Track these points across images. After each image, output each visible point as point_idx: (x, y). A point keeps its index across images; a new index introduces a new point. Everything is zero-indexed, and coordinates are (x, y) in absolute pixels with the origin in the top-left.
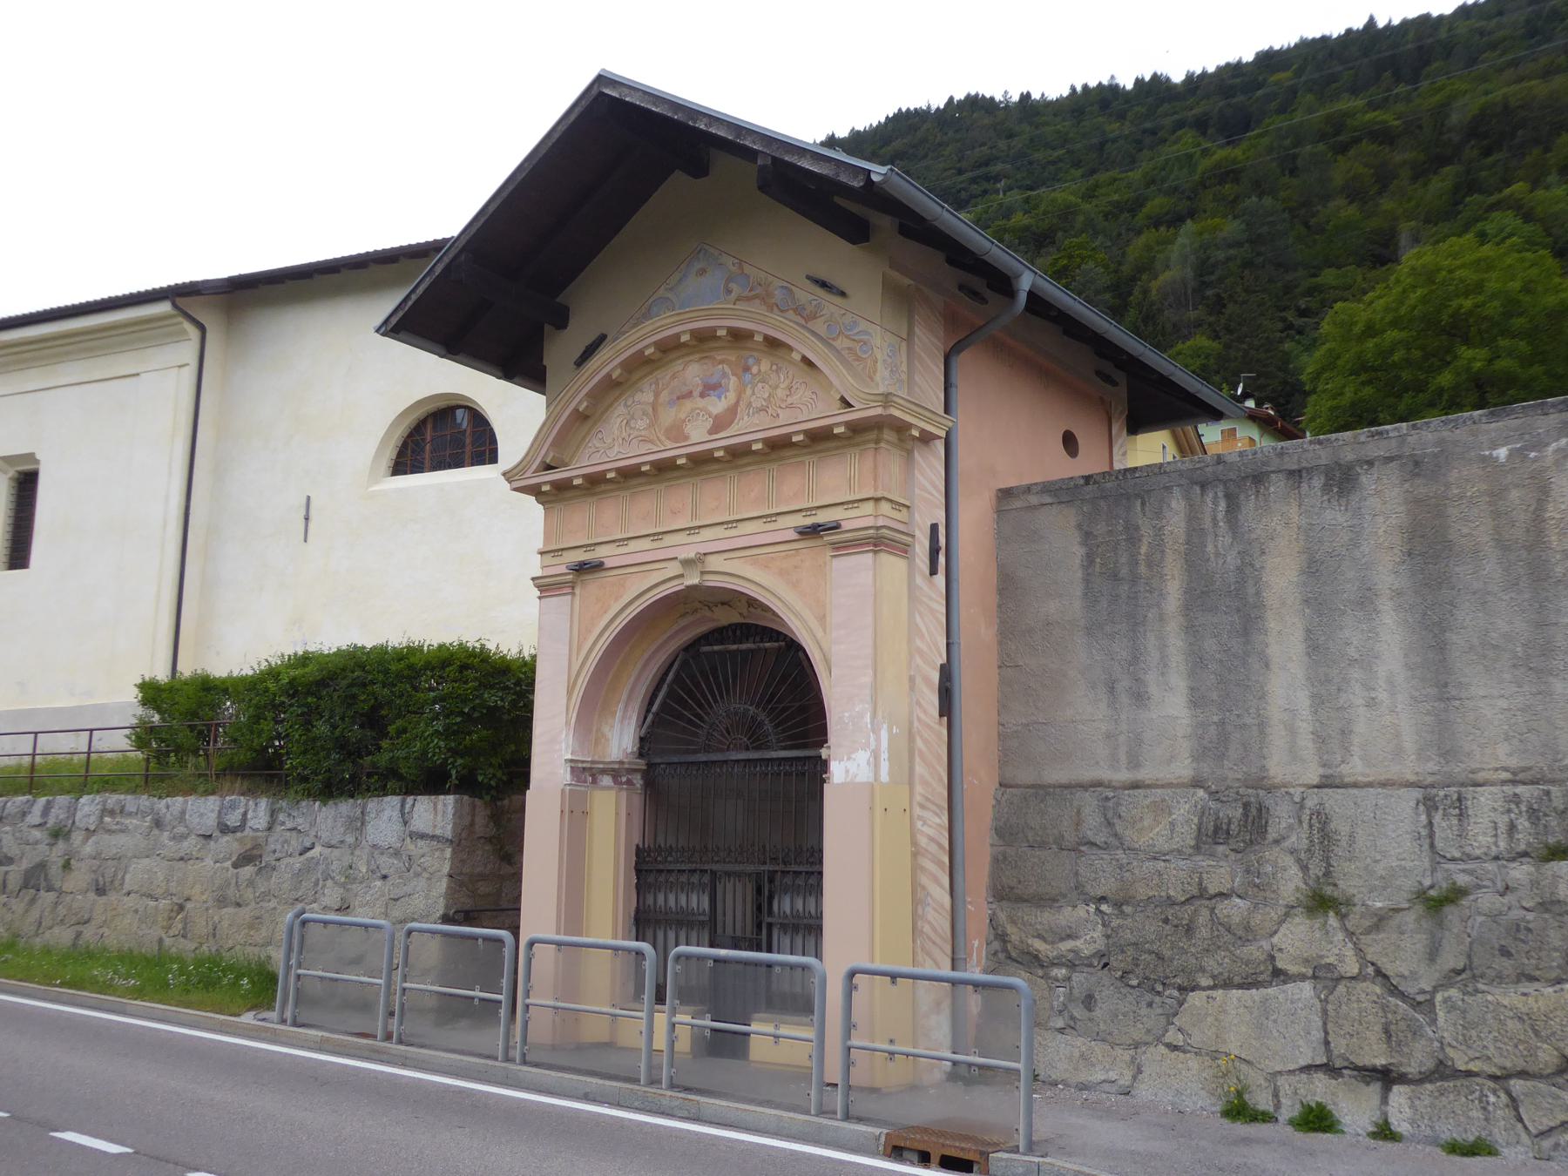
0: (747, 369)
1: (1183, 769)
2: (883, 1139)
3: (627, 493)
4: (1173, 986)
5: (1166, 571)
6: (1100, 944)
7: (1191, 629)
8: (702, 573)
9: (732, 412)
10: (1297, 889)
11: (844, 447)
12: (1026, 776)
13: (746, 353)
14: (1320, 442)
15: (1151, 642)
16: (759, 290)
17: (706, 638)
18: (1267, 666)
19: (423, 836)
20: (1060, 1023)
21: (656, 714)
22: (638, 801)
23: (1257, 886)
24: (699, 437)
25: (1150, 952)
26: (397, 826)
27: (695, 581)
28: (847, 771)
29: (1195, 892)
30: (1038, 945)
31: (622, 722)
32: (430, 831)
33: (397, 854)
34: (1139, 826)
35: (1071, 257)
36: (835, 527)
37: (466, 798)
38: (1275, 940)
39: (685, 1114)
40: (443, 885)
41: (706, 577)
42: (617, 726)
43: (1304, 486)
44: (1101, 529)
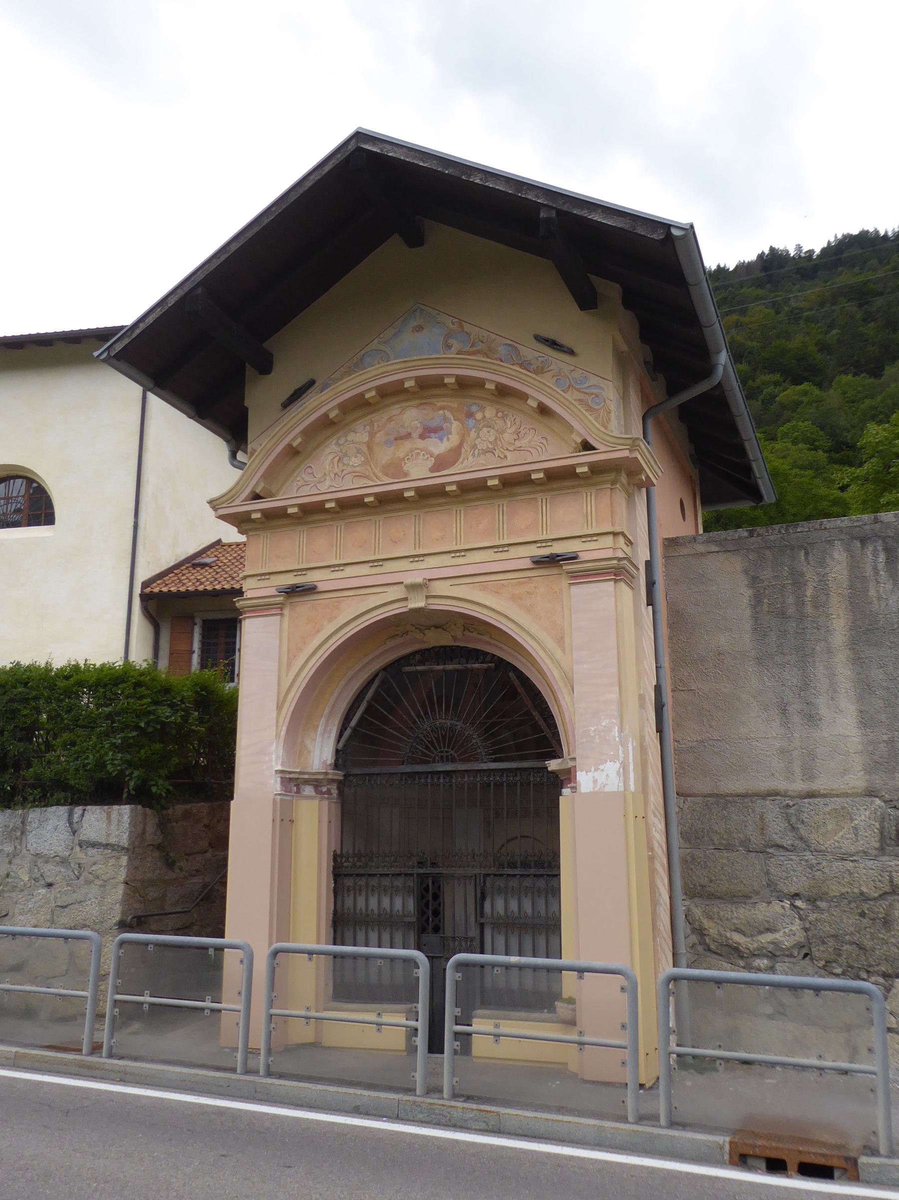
0: (470, 415)
1: (857, 780)
2: (727, 1147)
3: (342, 523)
4: (877, 973)
5: (831, 611)
6: (800, 937)
7: (857, 660)
8: (427, 597)
9: (455, 454)
11: (580, 486)
12: (703, 786)
13: (468, 401)
15: (820, 671)
16: (481, 346)
17: (406, 659)
19: (94, 845)
20: (769, 1010)
21: (354, 730)
22: (336, 810)
24: (419, 473)
26: (64, 835)
27: (421, 604)
28: (595, 781)
29: (887, 889)
30: (737, 937)
31: (323, 735)
32: (103, 840)
33: (64, 861)
34: (822, 830)
36: (573, 558)
37: (139, 807)
39: (483, 1126)
40: (120, 890)
41: (431, 601)
42: (319, 739)
44: (767, 574)
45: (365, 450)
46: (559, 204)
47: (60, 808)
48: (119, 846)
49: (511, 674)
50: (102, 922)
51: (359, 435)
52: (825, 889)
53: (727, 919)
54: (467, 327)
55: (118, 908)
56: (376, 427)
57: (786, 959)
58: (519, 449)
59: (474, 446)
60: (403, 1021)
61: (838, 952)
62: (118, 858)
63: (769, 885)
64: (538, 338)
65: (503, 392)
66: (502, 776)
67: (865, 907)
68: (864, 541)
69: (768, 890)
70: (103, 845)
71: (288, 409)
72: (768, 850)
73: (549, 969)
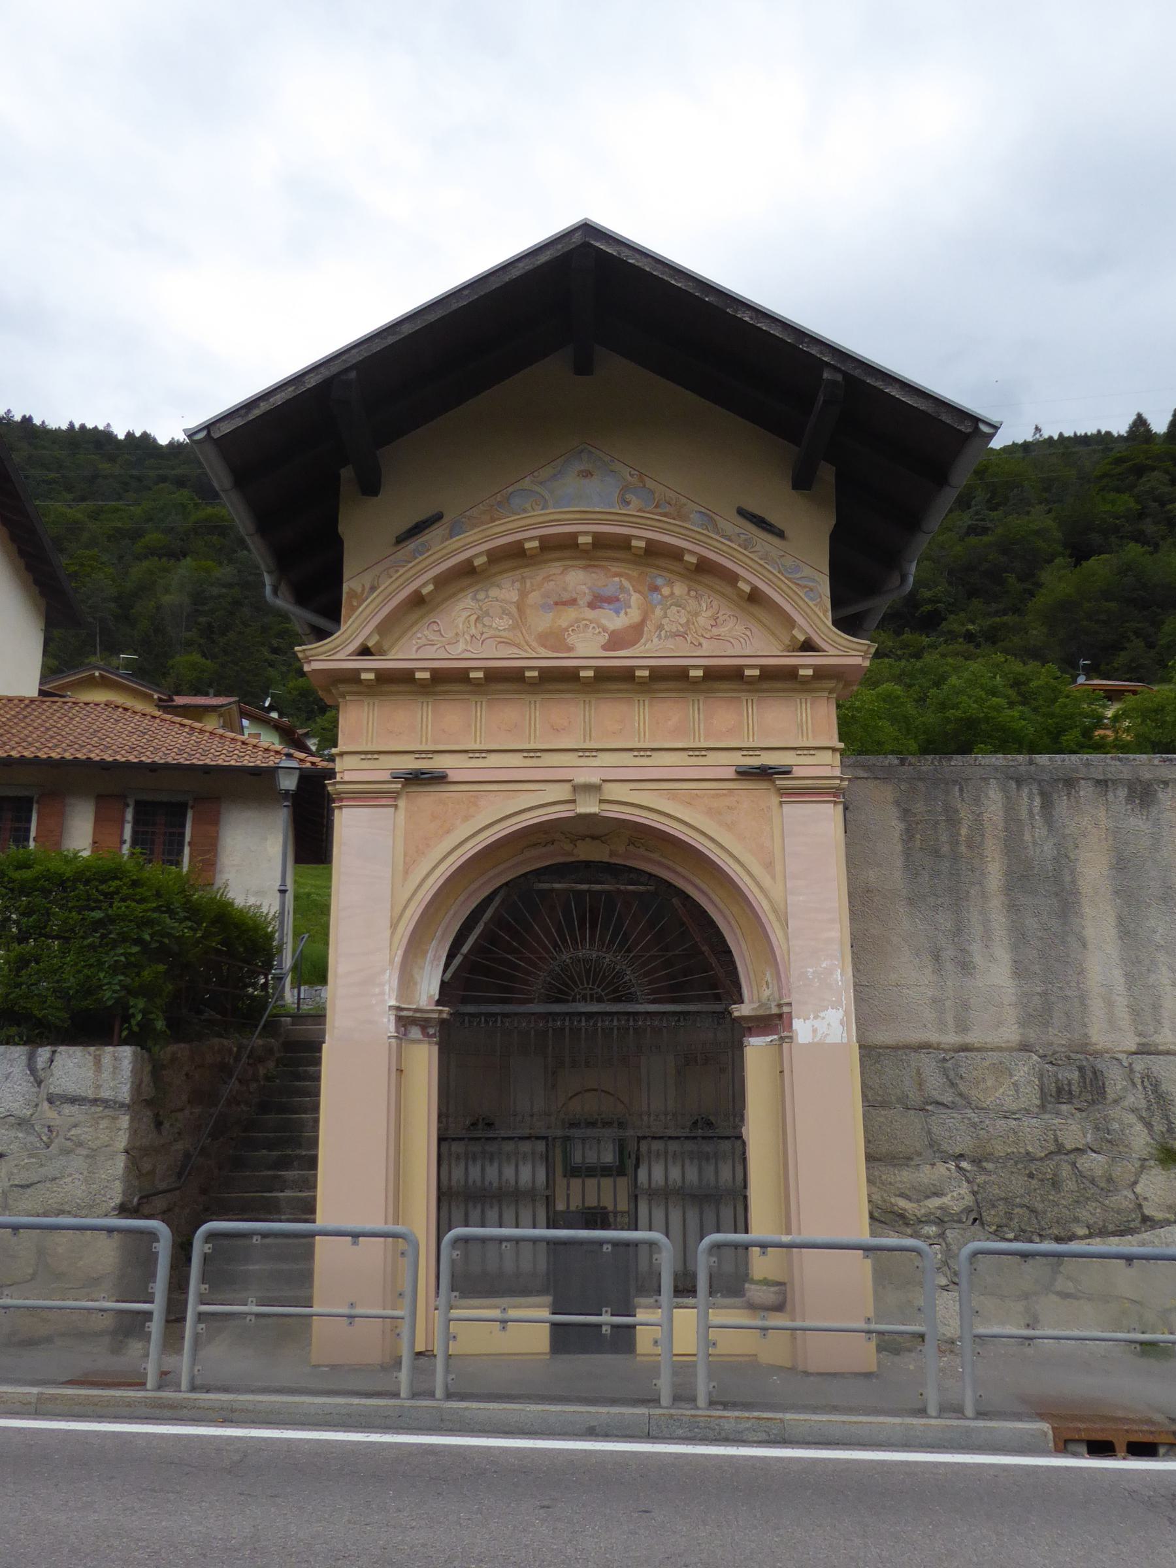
1: (1010, 1033)
6: (969, 1200)
7: (1013, 907)
9: (634, 634)
10: (1147, 1144)
14: (1120, 760)
16: (667, 509)
17: (539, 873)
18: (1084, 945)
19: (74, 1100)
23: (1110, 1142)
24: (587, 649)
25: (1022, 1206)
27: (593, 809)
28: (815, 1031)
29: (1052, 1148)
30: (902, 1203)
32: (90, 1094)
34: (982, 1086)
35: (82, 565)
36: (786, 772)
38: (1138, 1189)
39: (764, 1436)
40: (121, 1162)
42: (428, 967)
43: (1111, 796)
45: (514, 610)
46: (848, 367)
47: (13, 1048)
48: (115, 1103)
49: (675, 901)
50: (92, 1207)
51: (505, 591)
52: (989, 1150)
53: (890, 1183)
54: (650, 484)
55: (118, 1186)
56: (528, 584)
57: (955, 1225)
58: (717, 638)
59: (660, 627)
60: (545, 1314)
61: (1009, 1216)
62: (114, 1118)
63: (931, 1146)
64: (742, 512)
65: (705, 570)
66: (661, 1020)
67: (1033, 1167)
68: (1019, 782)
69: (930, 1151)
70: (90, 1101)
71: (401, 546)
72: (929, 1108)
73: (736, 1246)
